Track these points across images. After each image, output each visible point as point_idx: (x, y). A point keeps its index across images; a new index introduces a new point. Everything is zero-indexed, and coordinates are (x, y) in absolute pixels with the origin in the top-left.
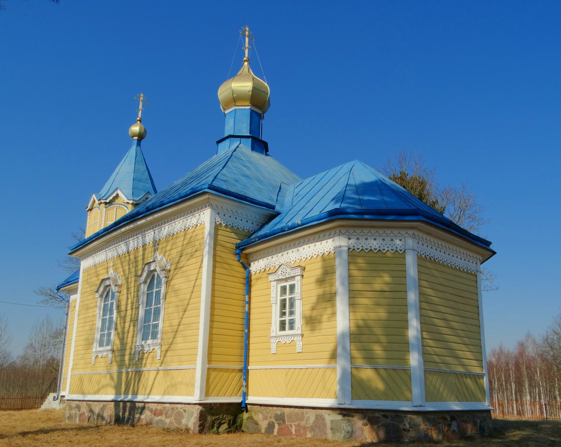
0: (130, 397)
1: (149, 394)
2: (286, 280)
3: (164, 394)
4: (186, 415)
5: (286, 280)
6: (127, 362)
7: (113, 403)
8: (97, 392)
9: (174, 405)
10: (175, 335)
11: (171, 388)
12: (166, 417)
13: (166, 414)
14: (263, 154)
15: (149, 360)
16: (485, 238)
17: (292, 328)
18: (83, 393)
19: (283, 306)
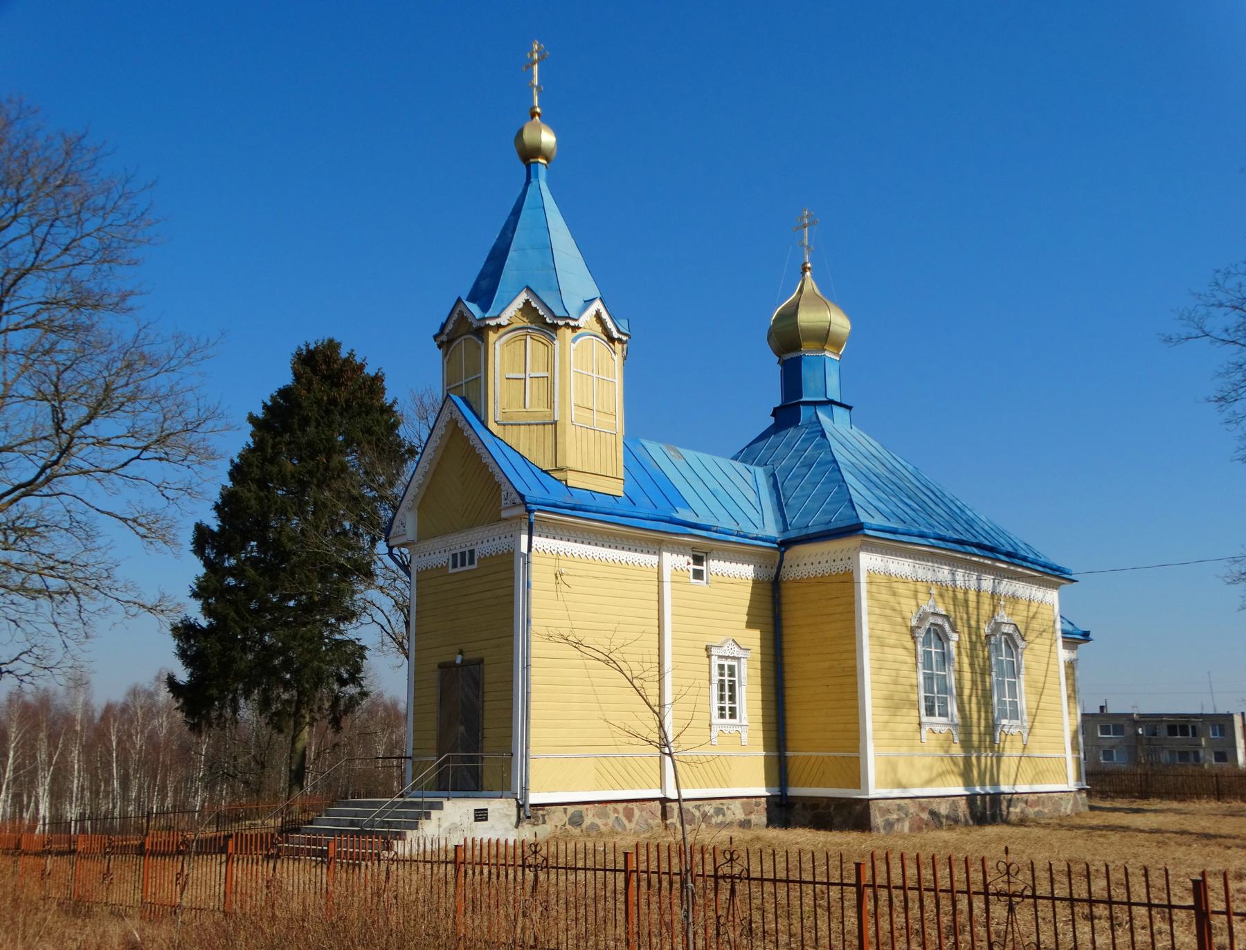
0: (989, 789)
1: (1014, 785)
2: (727, 658)
3: (1032, 783)
4: (1063, 803)
5: (727, 658)
6: (976, 743)
7: (965, 798)
8: (929, 782)
9: (1050, 794)
10: (1034, 719)
11: (1038, 777)
12: (1044, 807)
13: (1043, 803)
14: (799, 359)
15: (1007, 745)
16: (1215, 709)
17: (733, 716)
18: (900, 785)
19: (722, 688)
